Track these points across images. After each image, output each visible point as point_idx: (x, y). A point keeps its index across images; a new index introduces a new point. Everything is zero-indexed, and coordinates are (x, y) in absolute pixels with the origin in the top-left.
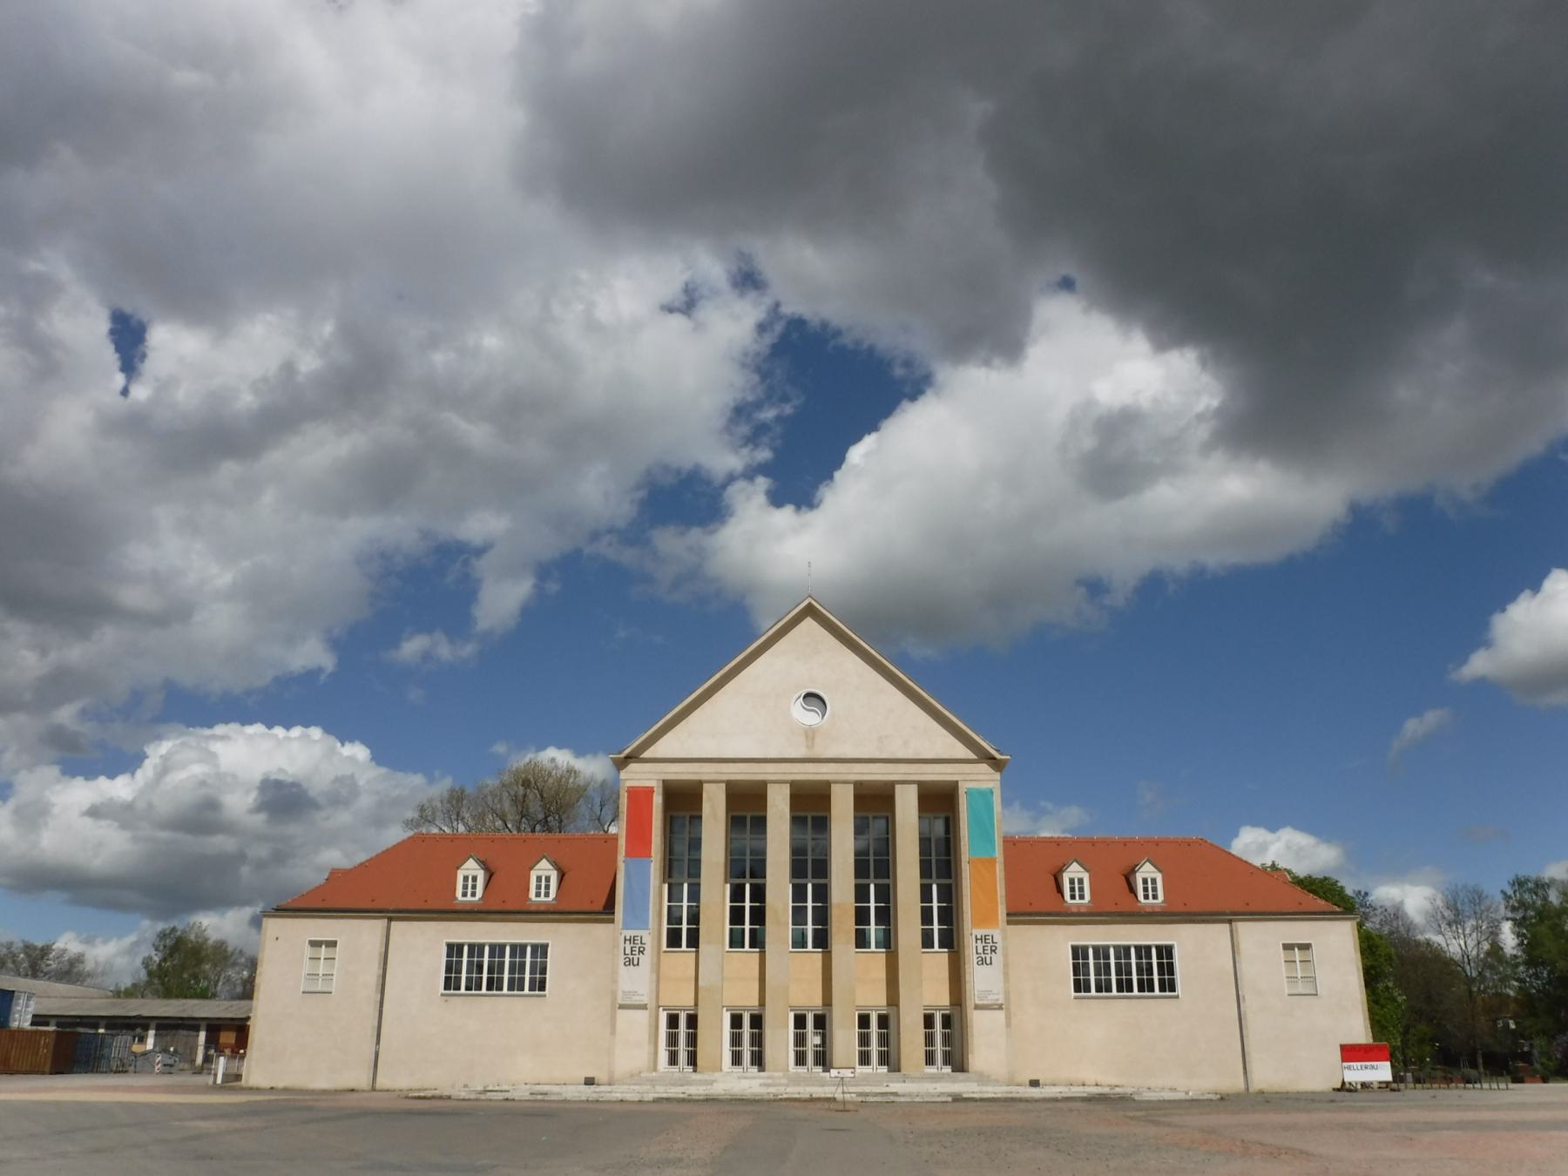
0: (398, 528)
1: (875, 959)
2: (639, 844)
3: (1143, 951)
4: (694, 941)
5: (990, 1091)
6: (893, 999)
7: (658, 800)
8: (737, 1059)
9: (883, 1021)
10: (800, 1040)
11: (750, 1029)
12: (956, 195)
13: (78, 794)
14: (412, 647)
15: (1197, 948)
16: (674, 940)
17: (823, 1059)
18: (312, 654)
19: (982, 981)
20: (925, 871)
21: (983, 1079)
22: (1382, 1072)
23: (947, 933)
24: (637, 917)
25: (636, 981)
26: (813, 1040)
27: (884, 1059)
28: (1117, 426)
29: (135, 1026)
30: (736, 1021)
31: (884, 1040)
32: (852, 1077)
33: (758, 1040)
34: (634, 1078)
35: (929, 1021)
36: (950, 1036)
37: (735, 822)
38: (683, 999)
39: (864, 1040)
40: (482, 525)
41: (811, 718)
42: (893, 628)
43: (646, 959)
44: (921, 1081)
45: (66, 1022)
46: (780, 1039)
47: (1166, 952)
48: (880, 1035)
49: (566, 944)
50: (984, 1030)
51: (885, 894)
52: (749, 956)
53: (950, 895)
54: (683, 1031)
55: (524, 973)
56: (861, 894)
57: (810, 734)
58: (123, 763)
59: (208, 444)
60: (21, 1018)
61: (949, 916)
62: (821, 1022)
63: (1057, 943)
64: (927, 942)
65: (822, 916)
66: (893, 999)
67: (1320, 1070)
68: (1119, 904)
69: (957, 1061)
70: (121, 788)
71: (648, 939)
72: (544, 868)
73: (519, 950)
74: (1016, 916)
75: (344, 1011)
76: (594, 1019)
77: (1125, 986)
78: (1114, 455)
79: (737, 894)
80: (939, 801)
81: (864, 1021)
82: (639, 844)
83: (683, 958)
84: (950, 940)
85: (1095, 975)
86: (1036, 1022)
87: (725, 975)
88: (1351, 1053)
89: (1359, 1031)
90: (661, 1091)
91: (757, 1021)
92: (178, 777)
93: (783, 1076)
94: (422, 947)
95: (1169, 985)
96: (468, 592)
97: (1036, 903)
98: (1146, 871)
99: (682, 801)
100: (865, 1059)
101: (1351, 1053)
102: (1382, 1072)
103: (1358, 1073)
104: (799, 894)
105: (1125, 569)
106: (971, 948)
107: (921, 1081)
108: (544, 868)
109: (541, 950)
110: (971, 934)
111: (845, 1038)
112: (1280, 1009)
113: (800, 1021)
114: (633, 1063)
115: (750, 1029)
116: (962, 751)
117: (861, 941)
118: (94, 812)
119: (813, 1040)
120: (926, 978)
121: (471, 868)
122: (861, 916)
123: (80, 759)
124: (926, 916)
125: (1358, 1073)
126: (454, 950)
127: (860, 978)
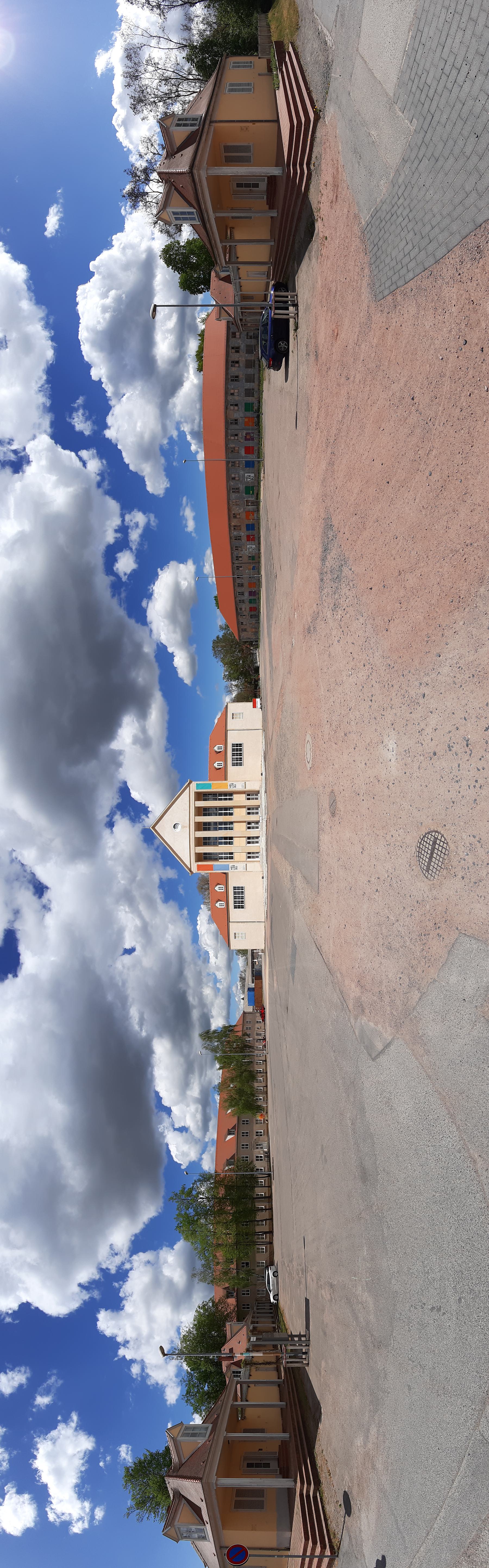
0: (157, 896)
1: (235, 811)
2: (210, 868)
3: (233, 750)
4: (232, 853)
5: (264, 785)
6: (244, 807)
7: (200, 863)
8: (257, 842)
9: (249, 809)
10: (253, 828)
11: (250, 840)
12: (87, 770)
13: (212, 960)
14: (181, 891)
15: (232, 738)
16: (232, 858)
17: (257, 822)
18: (185, 912)
19: (239, 787)
20: (216, 800)
21: (261, 787)
22: (258, 700)
23: (229, 795)
24: (227, 867)
25: (241, 866)
26: (253, 825)
27: (257, 809)
28: (136, 740)
29: (253, 964)
30: (249, 843)
31: (253, 809)
32: (261, 816)
33: (253, 838)
34: (262, 866)
35: (249, 799)
36: (251, 794)
37: (205, 844)
38: (244, 855)
39: (253, 813)
40: (156, 877)
41: (180, 827)
42: (173, 795)
43: (236, 864)
44: (262, 801)
45: (253, 975)
46: (253, 833)
47: (233, 745)
48: (251, 810)
49: (232, 884)
50: (250, 787)
51: (221, 809)
52: (235, 840)
53: (221, 794)
54: (250, 855)
55: (239, 892)
56: (221, 814)
57: (183, 827)
58: (207, 953)
59: (145, 931)
60: (253, 985)
61: (225, 795)
62: (249, 823)
63: (231, 769)
64: (230, 799)
65: (225, 823)
66: (244, 807)
67: (258, 713)
68: (223, 755)
69: (257, 793)
70: (211, 954)
71: (231, 865)
72: (217, 888)
73: (235, 893)
74: (226, 779)
75: (250, 929)
76: (249, 874)
77: (241, 755)
78: (143, 741)
79: (221, 843)
80: (200, 796)
81: (249, 813)
82: (210, 868)
83: (235, 856)
84: (231, 794)
85: (238, 762)
86: (248, 775)
87: (239, 846)
88: (254, 706)
89: (251, 704)
90: (265, 862)
91: (249, 838)
92: (208, 942)
93: (261, 832)
94: (235, 914)
95: (240, 745)
96: (170, 881)
97: (223, 774)
98: (216, 748)
99: (201, 857)
100: (257, 813)
101: (254, 706)
102: (258, 700)
103: (258, 705)
104: (221, 829)
105: (164, 742)
106: (232, 789)
107: (262, 801)
108: (217, 888)
109: (235, 888)
110: (229, 789)
111: (252, 818)
112: (244, 721)
113: (249, 828)
114: (258, 867)
115: (250, 840)
116: (188, 790)
117: (231, 814)
118: (217, 958)
119: (253, 825)
120: (239, 799)
121: (218, 905)
122: (226, 814)
123: (207, 960)
124: (226, 799)
125: (258, 705)
126: (235, 907)
127: (239, 814)
